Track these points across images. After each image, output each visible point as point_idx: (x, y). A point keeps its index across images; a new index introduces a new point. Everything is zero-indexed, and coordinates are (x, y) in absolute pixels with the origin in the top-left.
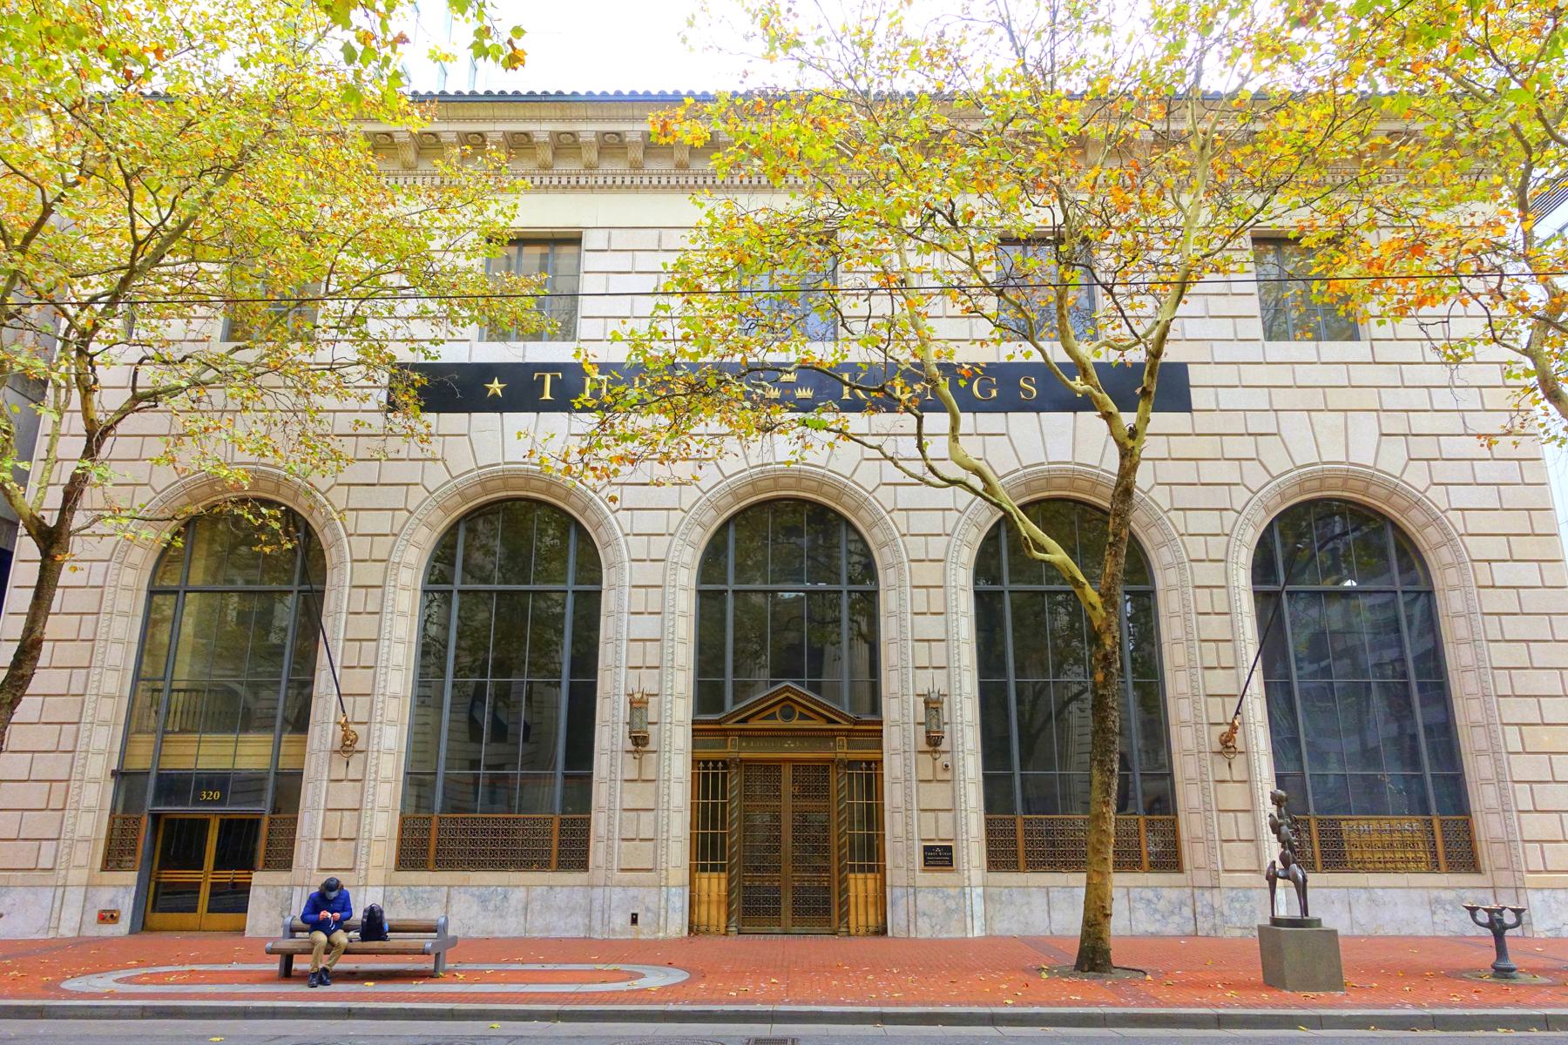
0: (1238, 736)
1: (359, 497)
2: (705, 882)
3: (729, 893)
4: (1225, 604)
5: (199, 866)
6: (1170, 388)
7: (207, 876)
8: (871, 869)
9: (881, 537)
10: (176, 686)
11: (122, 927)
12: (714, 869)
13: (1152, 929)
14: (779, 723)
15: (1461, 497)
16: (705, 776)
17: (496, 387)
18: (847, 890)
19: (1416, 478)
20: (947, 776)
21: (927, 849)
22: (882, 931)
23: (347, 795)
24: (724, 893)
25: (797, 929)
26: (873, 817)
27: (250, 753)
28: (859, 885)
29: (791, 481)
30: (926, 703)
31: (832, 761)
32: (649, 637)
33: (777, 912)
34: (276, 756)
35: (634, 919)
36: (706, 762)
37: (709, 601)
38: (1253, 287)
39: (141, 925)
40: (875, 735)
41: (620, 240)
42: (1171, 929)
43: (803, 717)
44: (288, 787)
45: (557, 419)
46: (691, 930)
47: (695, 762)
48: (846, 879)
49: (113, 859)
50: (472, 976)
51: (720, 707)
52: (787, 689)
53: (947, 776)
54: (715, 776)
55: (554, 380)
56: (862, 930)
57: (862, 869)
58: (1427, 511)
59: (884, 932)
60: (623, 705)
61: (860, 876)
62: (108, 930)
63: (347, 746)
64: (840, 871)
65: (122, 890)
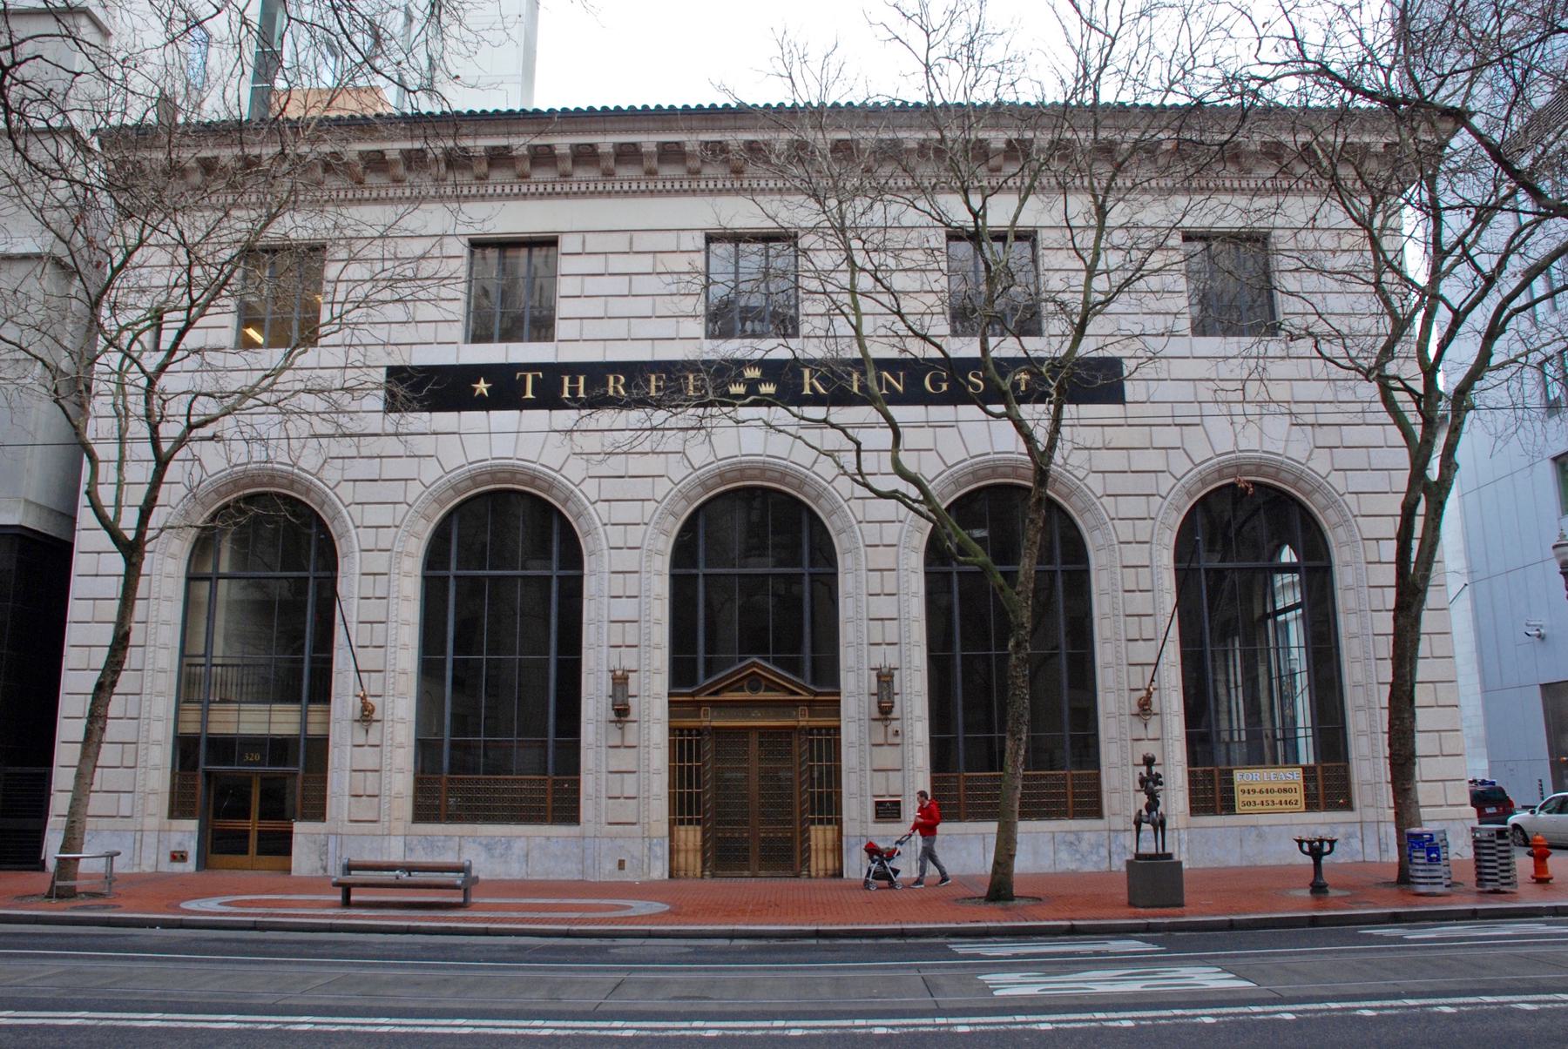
0: (1154, 699)
1: (365, 492)
2: (682, 834)
3: (704, 841)
4: (1148, 581)
5: (246, 815)
6: (1098, 381)
7: (253, 825)
8: (829, 822)
9: (839, 524)
10: (215, 661)
11: (190, 866)
12: (690, 822)
13: (1073, 866)
14: (745, 695)
15: (1358, 481)
16: (681, 742)
17: (482, 387)
18: (809, 839)
19: (1320, 464)
20: (897, 740)
21: (878, 804)
22: (838, 874)
23: (369, 758)
24: (699, 843)
25: (762, 873)
26: (833, 776)
27: (282, 720)
28: (820, 835)
29: (756, 472)
30: (879, 677)
31: (794, 728)
32: (626, 616)
33: (746, 859)
34: (304, 723)
35: (621, 865)
36: (681, 730)
37: (681, 588)
38: (1182, 284)
39: (203, 863)
40: (834, 707)
41: (593, 243)
42: (1088, 868)
43: (768, 689)
44: (318, 749)
45: (538, 418)
46: (671, 876)
47: (672, 730)
48: (808, 830)
49: (179, 807)
50: (484, 907)
51: (692, 681)
52: (754, 664)
53: (897, 740)
54: (690, 742)
55: (535, 378)
56: (821, 873)
57: (821, 822)
58: (1327, 495)
59: (841, 875)
60: (606, 686)
61: (820, 827)
62: (178, 867)
63: (366, 716)
64: (802, 824)
65: (187, 833)
